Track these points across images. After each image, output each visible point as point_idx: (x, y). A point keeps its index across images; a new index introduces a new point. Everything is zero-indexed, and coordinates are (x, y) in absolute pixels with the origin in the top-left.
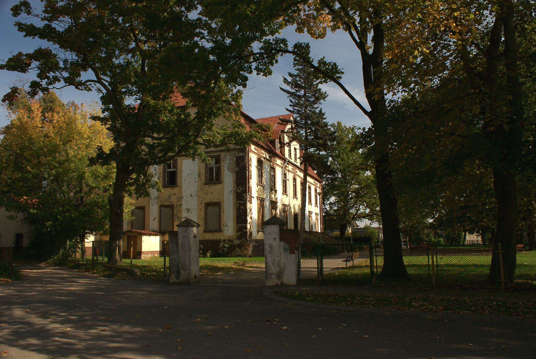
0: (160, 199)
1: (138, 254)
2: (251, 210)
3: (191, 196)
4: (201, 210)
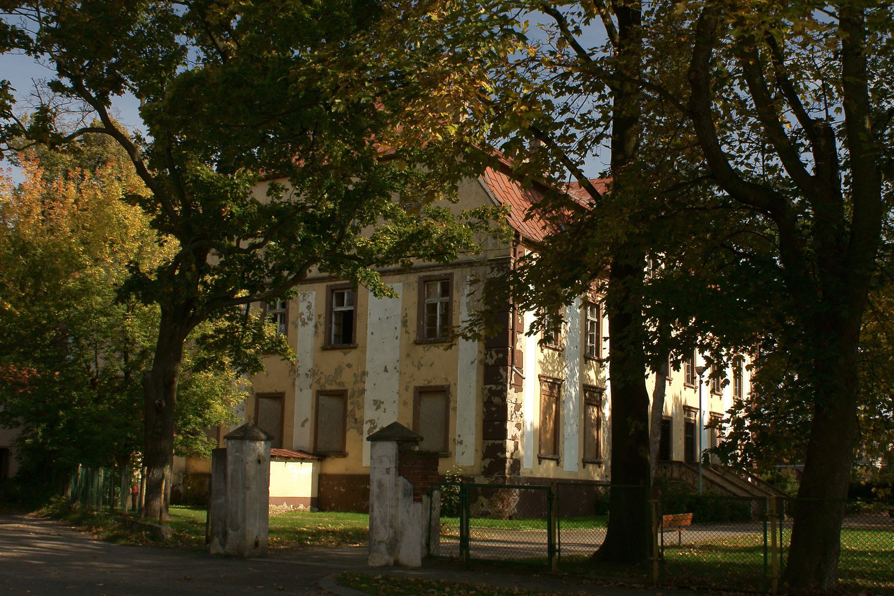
0: (317, 377)
2: (518, 407)
3: (386, 370)
4: (405, 403)
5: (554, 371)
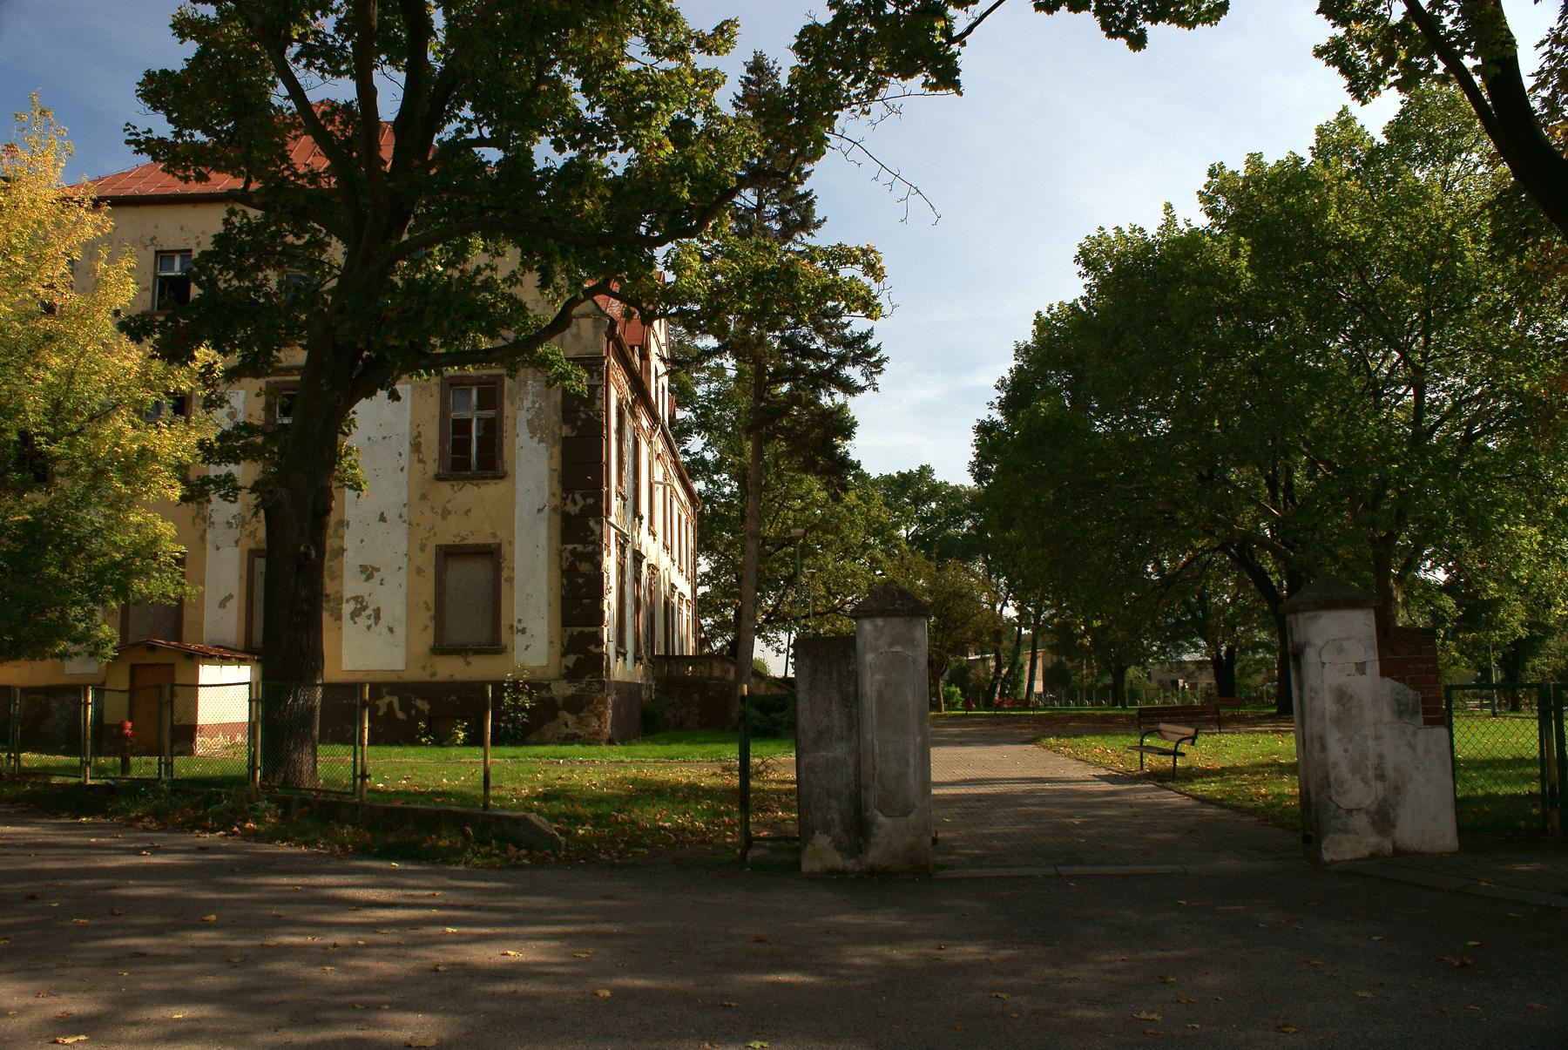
1: (186, 733)
4: (420, 571)
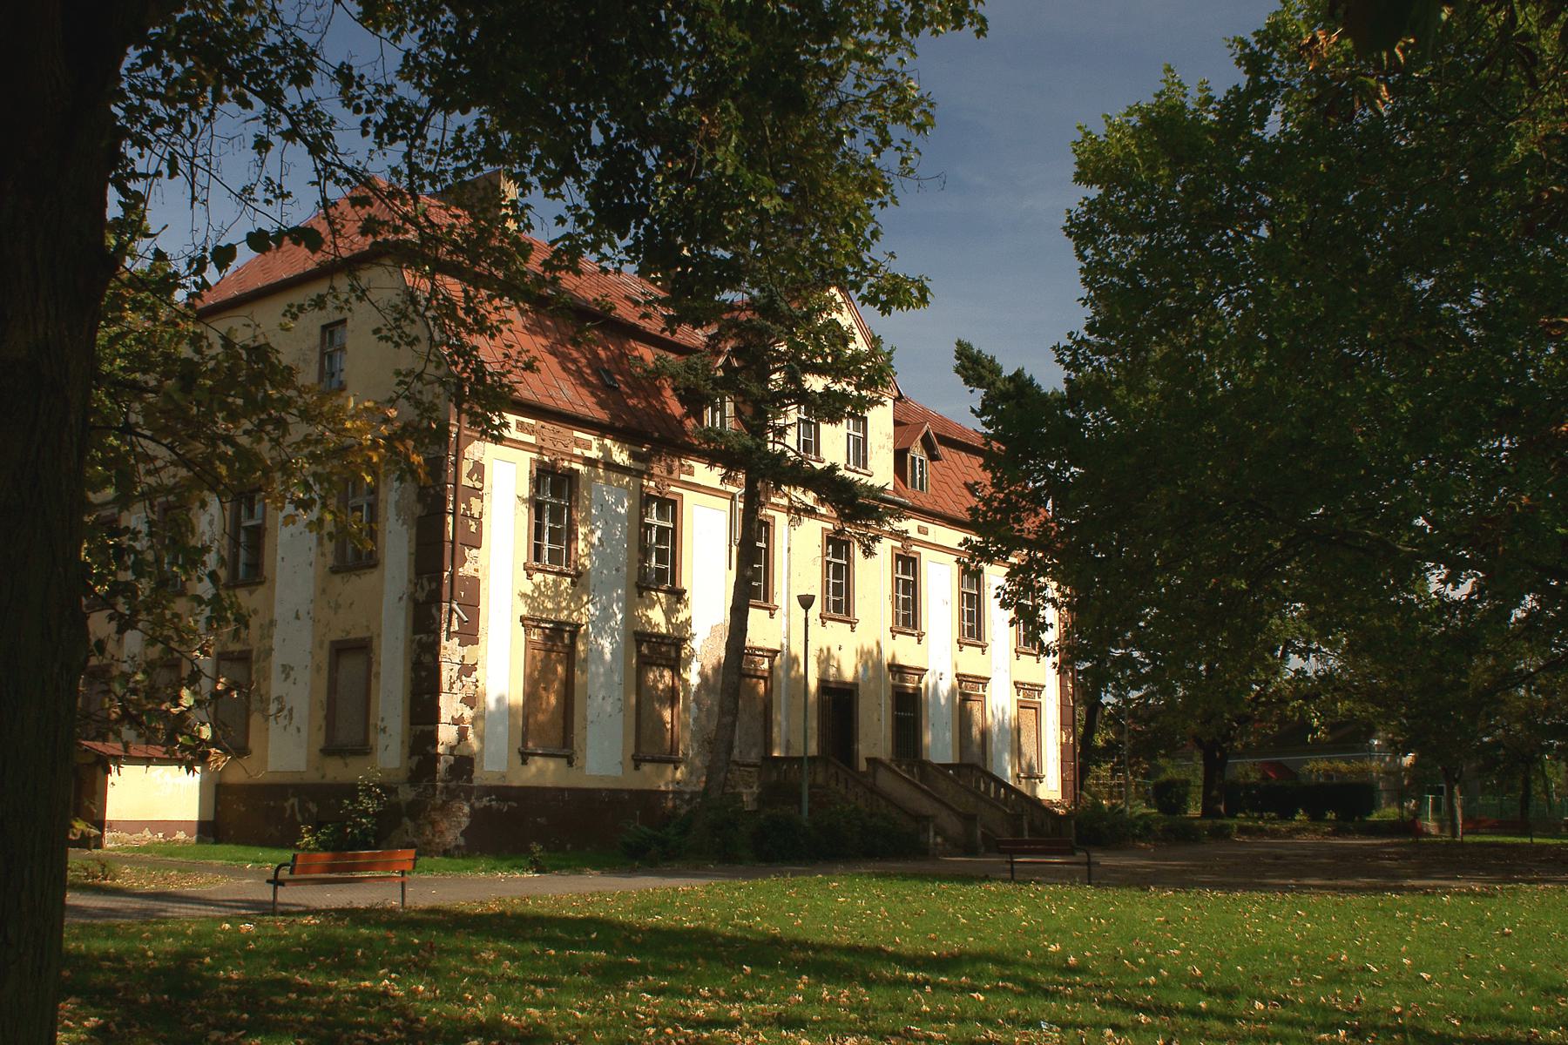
2: (467, 670)
3: (297, 617)
5: (559, 610)
